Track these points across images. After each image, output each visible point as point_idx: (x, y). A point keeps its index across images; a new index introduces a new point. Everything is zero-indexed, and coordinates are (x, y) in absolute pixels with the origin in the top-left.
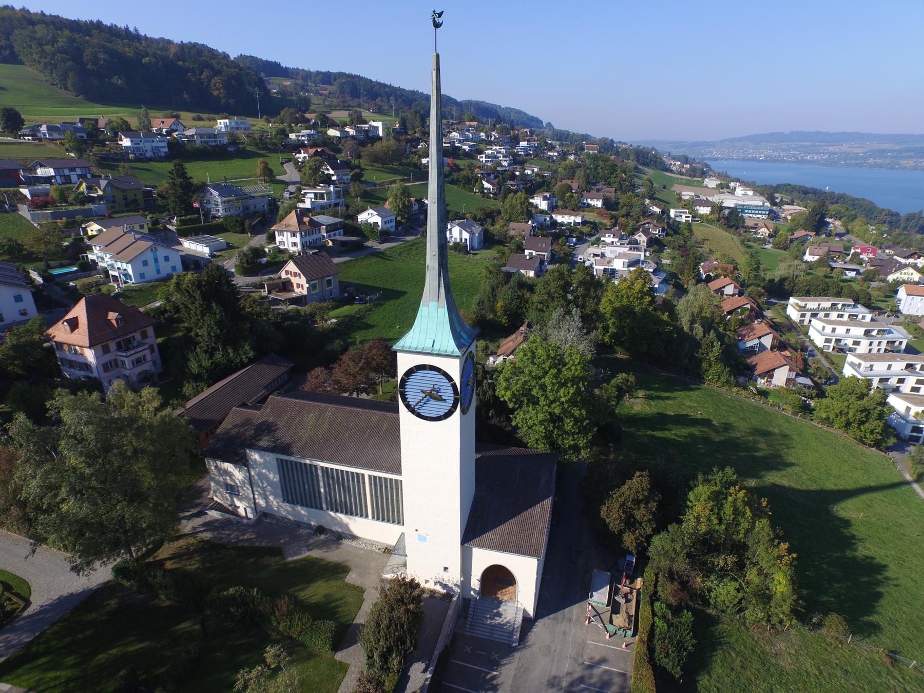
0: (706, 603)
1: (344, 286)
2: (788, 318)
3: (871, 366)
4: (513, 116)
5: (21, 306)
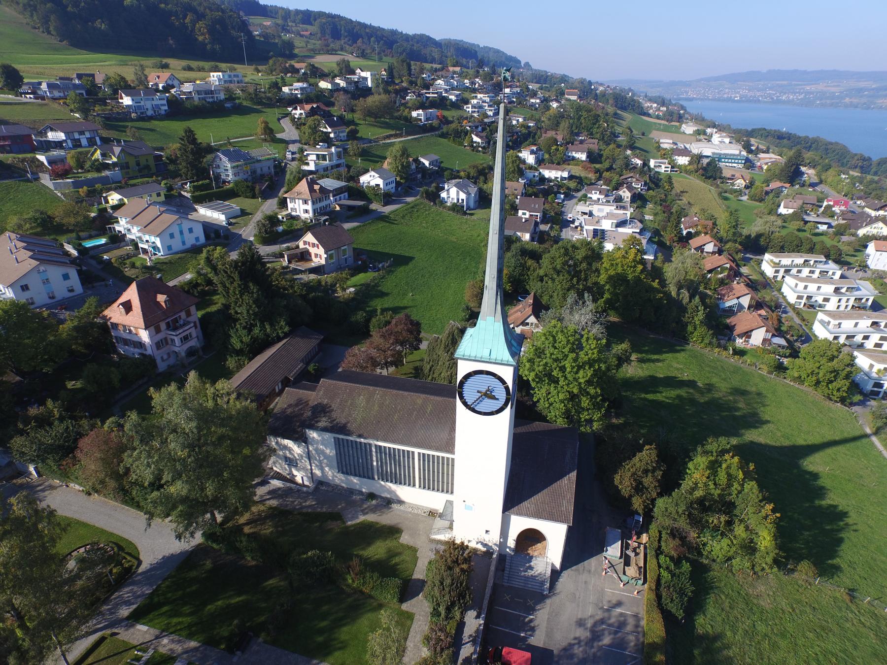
0: (700, 554)
1: (358, 253)
2: (762, 274)
3: (840, 324)
4: (492, 57)
5: (68, 283)
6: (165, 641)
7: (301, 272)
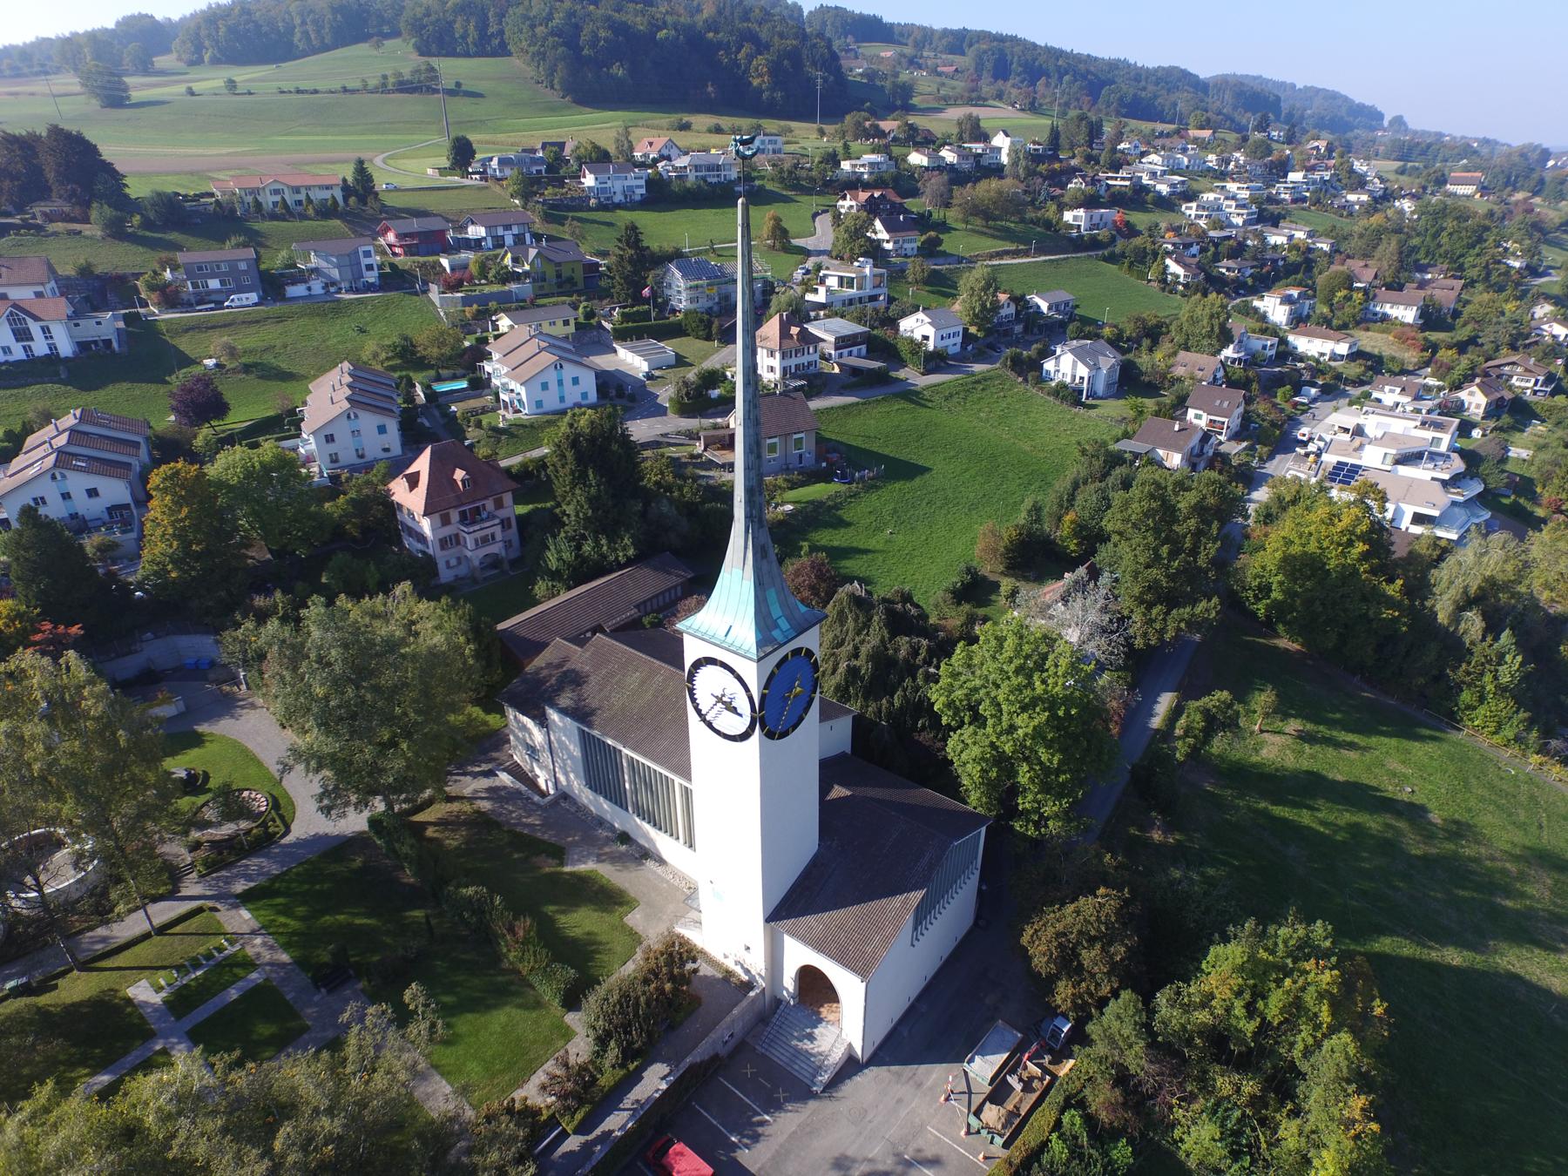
6: (258, 941)
7: (717, 466)
